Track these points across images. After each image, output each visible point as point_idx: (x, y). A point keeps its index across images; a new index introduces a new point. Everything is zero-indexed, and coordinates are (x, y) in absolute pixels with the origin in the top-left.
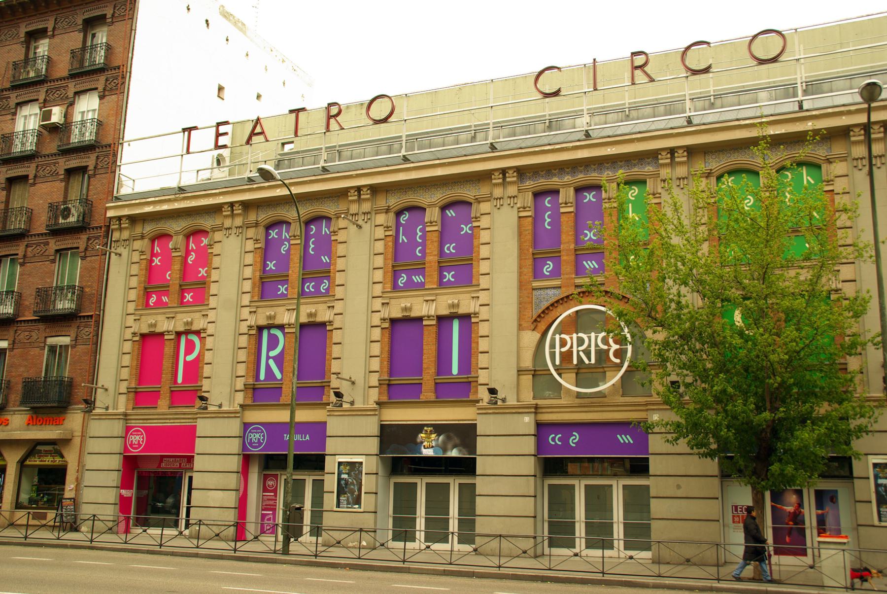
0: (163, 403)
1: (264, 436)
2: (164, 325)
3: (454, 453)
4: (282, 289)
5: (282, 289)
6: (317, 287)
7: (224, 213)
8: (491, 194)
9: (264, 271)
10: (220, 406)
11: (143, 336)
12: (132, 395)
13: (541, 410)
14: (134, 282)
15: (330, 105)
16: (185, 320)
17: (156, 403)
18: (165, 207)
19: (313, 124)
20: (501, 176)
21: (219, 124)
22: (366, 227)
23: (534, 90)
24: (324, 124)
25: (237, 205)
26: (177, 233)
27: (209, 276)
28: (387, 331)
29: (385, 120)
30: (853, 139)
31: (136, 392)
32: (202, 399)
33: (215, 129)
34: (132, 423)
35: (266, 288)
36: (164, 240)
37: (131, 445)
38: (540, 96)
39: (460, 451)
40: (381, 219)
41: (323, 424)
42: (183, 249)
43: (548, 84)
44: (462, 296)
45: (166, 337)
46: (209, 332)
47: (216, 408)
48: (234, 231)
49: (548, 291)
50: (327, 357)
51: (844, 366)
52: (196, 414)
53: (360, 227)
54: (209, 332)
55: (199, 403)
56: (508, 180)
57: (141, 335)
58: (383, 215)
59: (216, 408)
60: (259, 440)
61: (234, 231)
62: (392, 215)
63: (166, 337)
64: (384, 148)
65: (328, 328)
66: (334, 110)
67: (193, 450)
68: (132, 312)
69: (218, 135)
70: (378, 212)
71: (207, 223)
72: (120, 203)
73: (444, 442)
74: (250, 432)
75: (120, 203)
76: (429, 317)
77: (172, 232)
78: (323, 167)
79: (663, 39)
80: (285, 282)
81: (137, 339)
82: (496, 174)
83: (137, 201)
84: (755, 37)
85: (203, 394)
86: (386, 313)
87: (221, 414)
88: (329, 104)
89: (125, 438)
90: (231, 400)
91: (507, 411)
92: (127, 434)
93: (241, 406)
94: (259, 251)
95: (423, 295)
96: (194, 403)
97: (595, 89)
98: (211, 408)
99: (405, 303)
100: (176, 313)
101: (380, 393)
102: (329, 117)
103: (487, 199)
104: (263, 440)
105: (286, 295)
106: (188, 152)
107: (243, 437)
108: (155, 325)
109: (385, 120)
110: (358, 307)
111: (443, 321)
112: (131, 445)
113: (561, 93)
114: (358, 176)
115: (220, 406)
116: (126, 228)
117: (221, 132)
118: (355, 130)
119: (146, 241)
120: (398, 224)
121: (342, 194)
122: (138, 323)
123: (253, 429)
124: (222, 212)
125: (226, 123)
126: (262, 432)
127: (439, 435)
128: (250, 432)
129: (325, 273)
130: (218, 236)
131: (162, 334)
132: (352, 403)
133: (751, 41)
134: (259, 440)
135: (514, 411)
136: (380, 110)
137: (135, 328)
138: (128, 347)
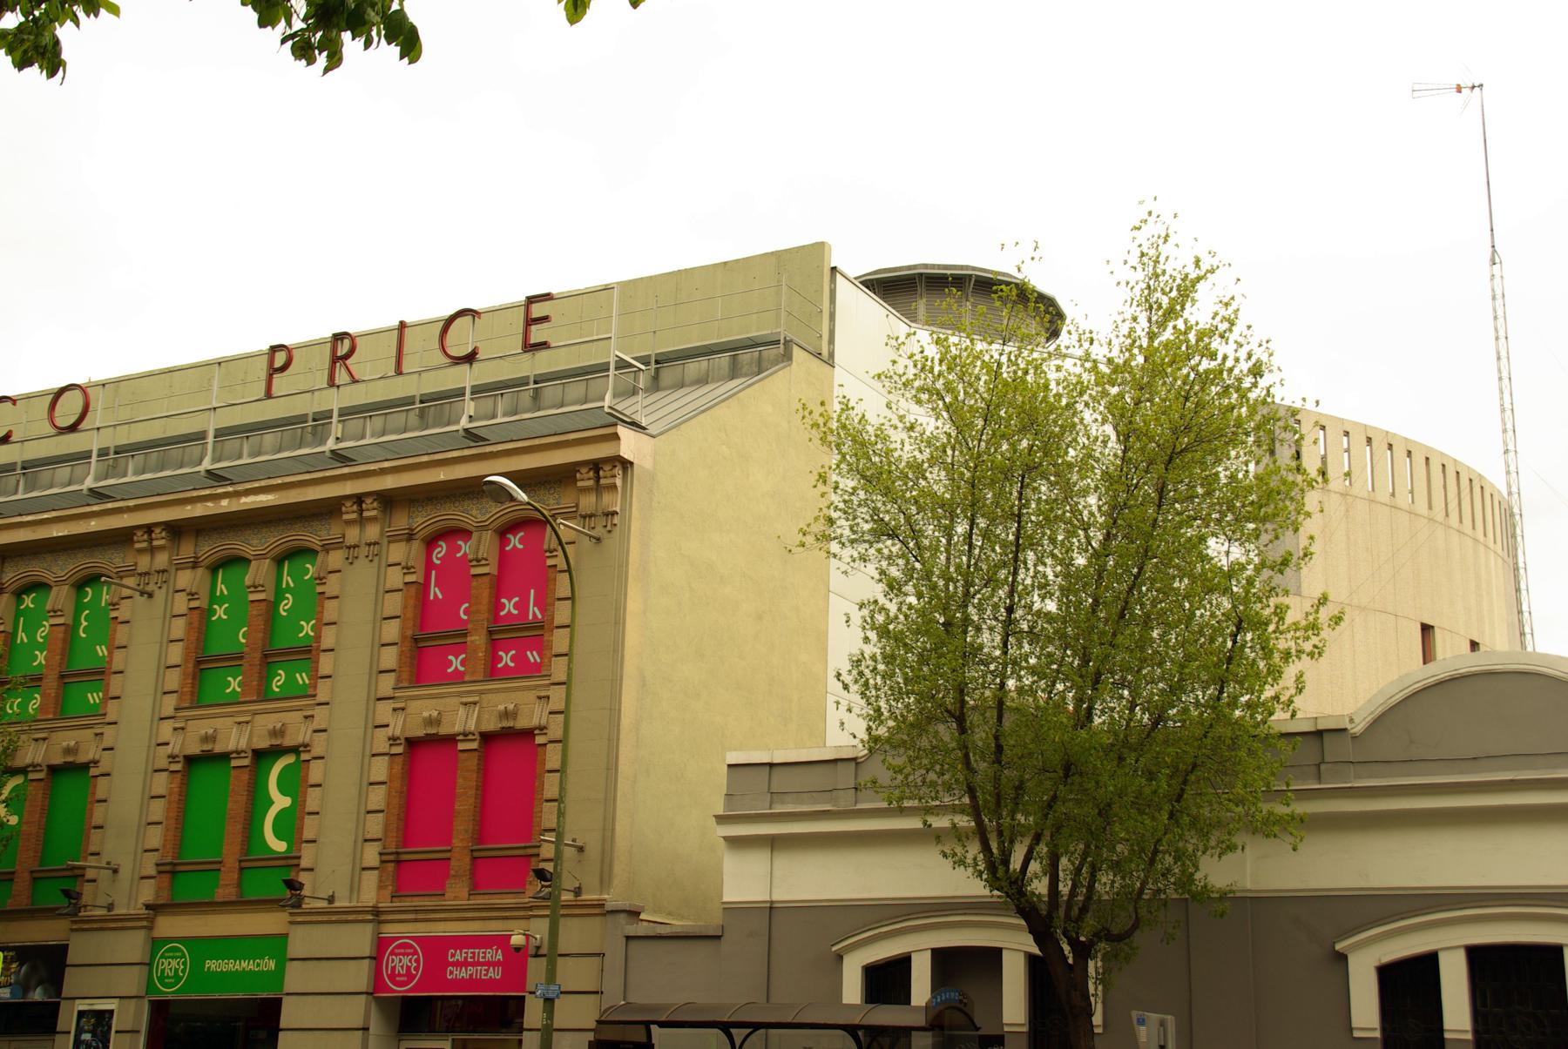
0: (457, 892)
1: (417, 961)
2: (234, 738)
3: (37, 995)
4: (456, 663)
5: (456, 663)
6: (520, 659)
7: (137, 546)
8: (577, 506)
9: (497, 618)
10: (331, 899)
11: (412, 743)
12: (391, 867)
13: (384, 917)
14: (392, 631)
15: (274, 349)
16: (426, 714)
17: (442, 887)
18: (441, 475)
19: (422, 352)
20: (591, 474)
21: (531, 300)
22: (160, 595)
23: (437, 345)
24: (263, 385)
25: (369, 501)
26: (60, 583)
27: (318, 638)
28: (399, 760)
29: (73, 428)
30: (580, 484)
31: (398, 862)
32: (541, 875)
33: (265, 359)
34: (390, 930)
35: (424, 659)
36: (235, 571)
37: (392, 977)
38: (53, 431)
39: (46, 991)
40: (397, 552)
41: (63, 950)
42: (270, 586)
43: (460, 341)
44: (219, 723)
45: (461, 746)
46: (317, 751)
47: (324, 904)
48: (364, 550)
49: (448, 700)
50: (537, 797)
51: (295, 862)
52: (531, 908)
53: (150, 595)
54: (317, 751)
55: (534, 886)
56: (366, 514)
57: (186, 757)
58: (188, 572)
59: (324, 904)
60: (408, 968)
61: (364, 550)
62: (417, 547)
63: (461, 746)
64: (526, 397)
65: (539, 740)
66: (343, 349)
67: (523, 989)
68: (390, 693)
69: (530, 322)
70: (393, 539)
71: (311, 536)
72: (110, 506)
73: (27, 975)
74: (392, 953)
75: (110, 506)
76: (238, 752)
77: (49, 577)
78: (466, 430)
79: (306, 326)
80: (459, 648)
81: (399, 750)
82: (584, 470)
83: (279, 481)
84: (62, 391)
85: (542, 865)
86: (397, 727)
87: (335, 916)
88: (529, 298)
89: (149, 965)
90: (355, 888)
91: (334, 918)
92: (152, 957)
93: (148, 907)
94: (413, 589)
95: (460, 694)
96: (523, 885)
97: (399, 372)
98: (309, 904)
99: (206, 727)
100: (255, 713)
101: (159, 889)
102: (335, 359)
103: (338, 545)
104: (417, 969)
105: (462, 674)
106: (399, 372)
107: (377, 958)
108: (437, 722)
109: (73, 428)
110: (353, 713)
111: (263, 757)
112: (392, 977)
113: (13, 439)
114: (383, 472)
115: (331, 899)
116: (161, 548)
117: (535, 315)
118: (302, 393)
119: (200, 571)
120: (429, 565)
121: (122, 538)
122: (180, 734)
123: (169, 950)
124: (341, 513)
125: (547, 297)
126: (416, 953)
127: (21, 965)
128: (392, 953)
129: (533, 635)
130: (335, 558)
131: (451, 740)
132: (578, 892)
133: (445, 330)
134: (408, 968)
135: (334, 918)
136: (68, 410)
137: (176, 747)
138: (380, 769)
